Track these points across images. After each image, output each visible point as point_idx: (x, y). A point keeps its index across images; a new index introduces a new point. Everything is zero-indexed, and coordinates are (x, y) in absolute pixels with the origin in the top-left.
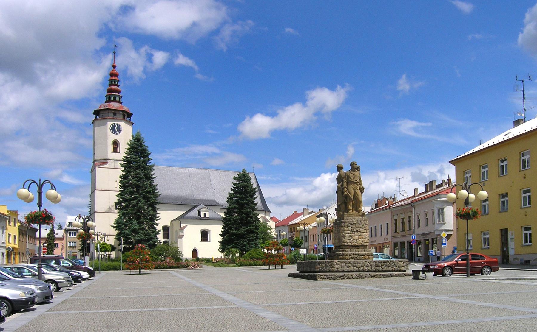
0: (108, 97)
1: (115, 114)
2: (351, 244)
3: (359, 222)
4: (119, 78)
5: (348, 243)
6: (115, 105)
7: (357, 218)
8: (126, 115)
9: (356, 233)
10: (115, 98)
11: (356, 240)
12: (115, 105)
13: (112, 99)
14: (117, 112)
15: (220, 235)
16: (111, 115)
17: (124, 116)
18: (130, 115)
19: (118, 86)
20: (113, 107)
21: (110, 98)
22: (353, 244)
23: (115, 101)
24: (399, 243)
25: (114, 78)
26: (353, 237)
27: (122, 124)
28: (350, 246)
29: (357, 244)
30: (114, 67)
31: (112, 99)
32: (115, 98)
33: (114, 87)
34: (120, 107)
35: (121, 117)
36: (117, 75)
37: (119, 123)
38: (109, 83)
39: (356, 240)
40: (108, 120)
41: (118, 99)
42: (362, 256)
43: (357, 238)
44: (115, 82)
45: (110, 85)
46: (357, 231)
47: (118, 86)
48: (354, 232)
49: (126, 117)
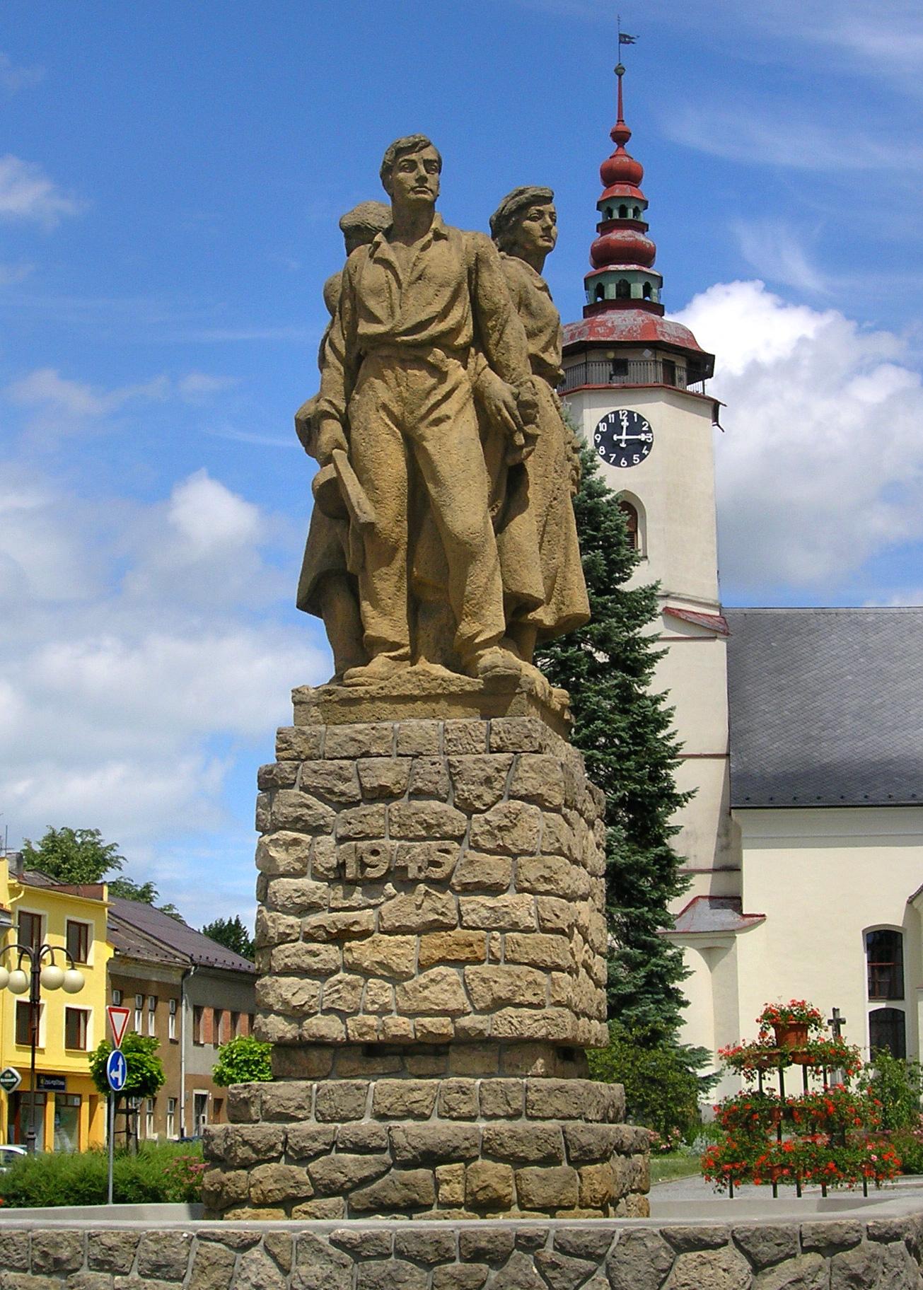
0: (593, 286)
1: (620, 367)
2: (329, 1027)
3: (431, 773)
4: (645, 189)
5: (297, 1015)
6: (623, 323)
7: (419, 727)
8: (681, 363)
9: (398, 906)
10: (623, 290)
11: (396, 978)
12: (623, 323)
13: (611, 292)
14: (630, 356)
15: (844, 1023)
16: (600, 371)
17: (669, 368)
18: (701, 365)
19: (643, 228)
20: (612, 330)
21: (600, 291)
22: (365, 1026)
23: (624, 301)
24: (895, 1005)
25: (620, 190)
26: (362, 952)
27: (658, 413)
28: (320, 1043)
29: (400, 1026)
30: (621, 138)
31: (611, 292)
32: (623, 290)
33: (617, 236)
34: (644, 328)
35: (654, 374)
36: (633, 178)
37: (640, 408)
38: (599, 217)
39: (396, 978)
40: (586, 399)
41: (637, 291)
42: (430, 1158)
43: (402, 952)
44: (623, 211)
45: (604, 228)
46: (400, 877)
47: (643, 228)
48: (372, 885)
49: (680, 373)
